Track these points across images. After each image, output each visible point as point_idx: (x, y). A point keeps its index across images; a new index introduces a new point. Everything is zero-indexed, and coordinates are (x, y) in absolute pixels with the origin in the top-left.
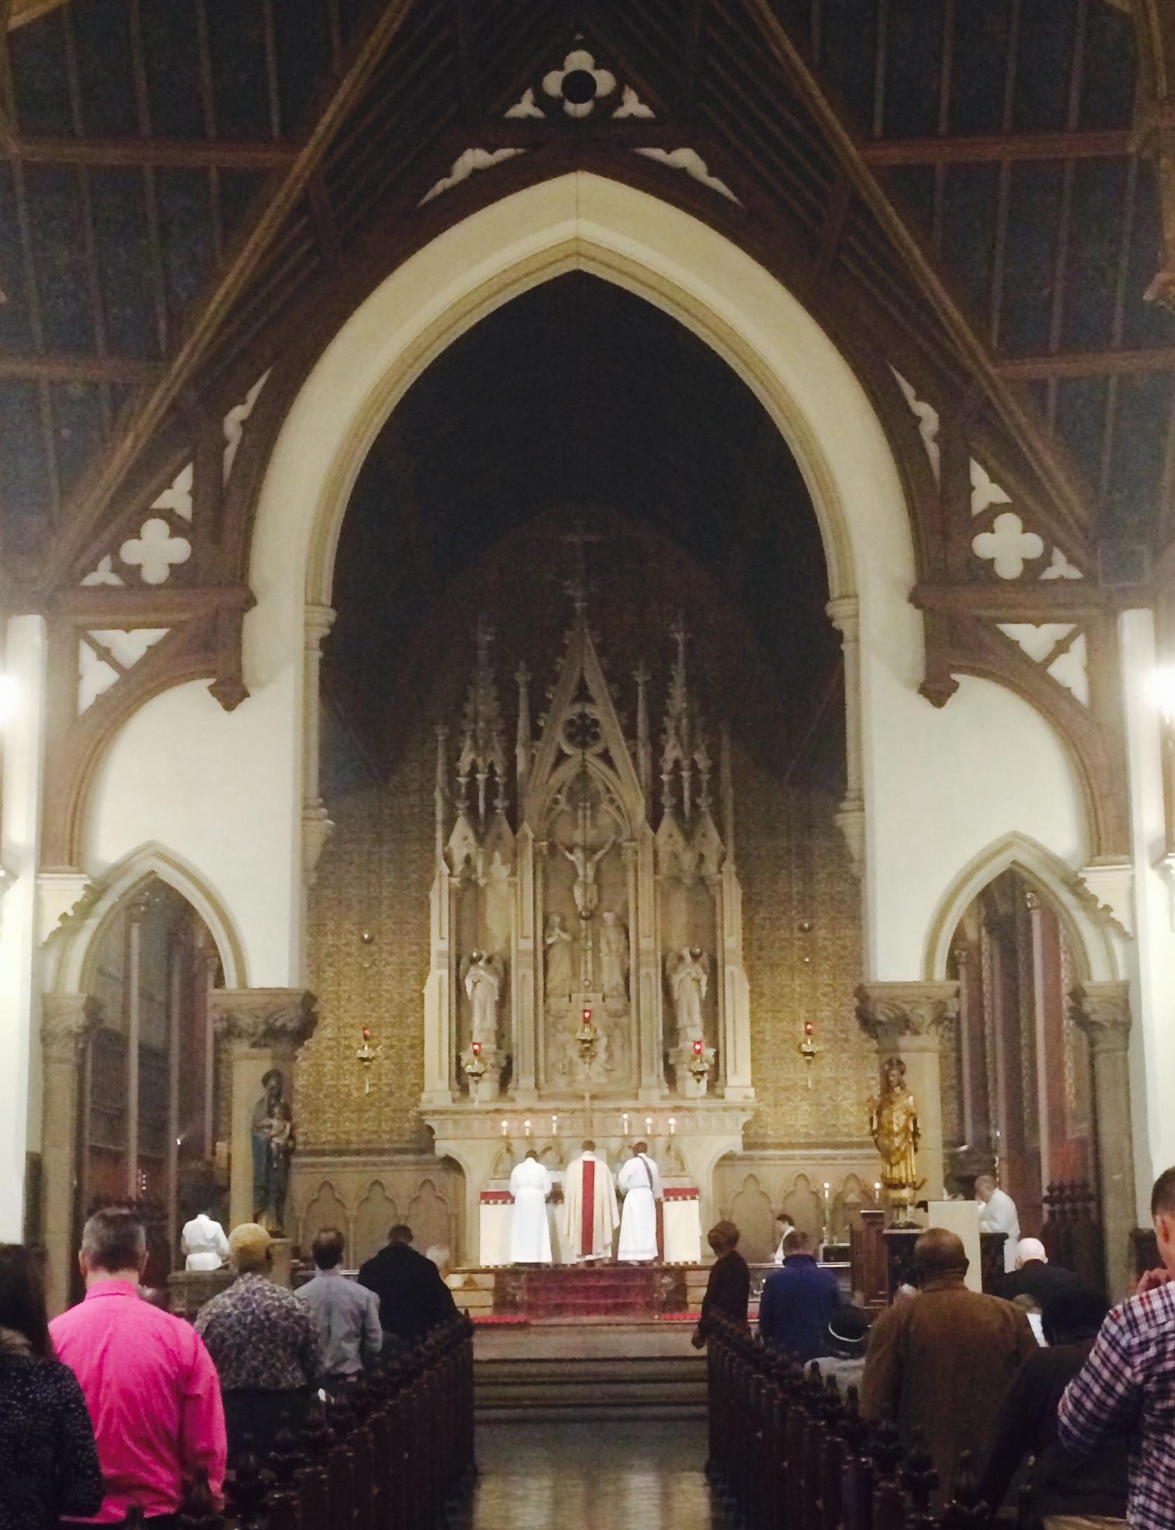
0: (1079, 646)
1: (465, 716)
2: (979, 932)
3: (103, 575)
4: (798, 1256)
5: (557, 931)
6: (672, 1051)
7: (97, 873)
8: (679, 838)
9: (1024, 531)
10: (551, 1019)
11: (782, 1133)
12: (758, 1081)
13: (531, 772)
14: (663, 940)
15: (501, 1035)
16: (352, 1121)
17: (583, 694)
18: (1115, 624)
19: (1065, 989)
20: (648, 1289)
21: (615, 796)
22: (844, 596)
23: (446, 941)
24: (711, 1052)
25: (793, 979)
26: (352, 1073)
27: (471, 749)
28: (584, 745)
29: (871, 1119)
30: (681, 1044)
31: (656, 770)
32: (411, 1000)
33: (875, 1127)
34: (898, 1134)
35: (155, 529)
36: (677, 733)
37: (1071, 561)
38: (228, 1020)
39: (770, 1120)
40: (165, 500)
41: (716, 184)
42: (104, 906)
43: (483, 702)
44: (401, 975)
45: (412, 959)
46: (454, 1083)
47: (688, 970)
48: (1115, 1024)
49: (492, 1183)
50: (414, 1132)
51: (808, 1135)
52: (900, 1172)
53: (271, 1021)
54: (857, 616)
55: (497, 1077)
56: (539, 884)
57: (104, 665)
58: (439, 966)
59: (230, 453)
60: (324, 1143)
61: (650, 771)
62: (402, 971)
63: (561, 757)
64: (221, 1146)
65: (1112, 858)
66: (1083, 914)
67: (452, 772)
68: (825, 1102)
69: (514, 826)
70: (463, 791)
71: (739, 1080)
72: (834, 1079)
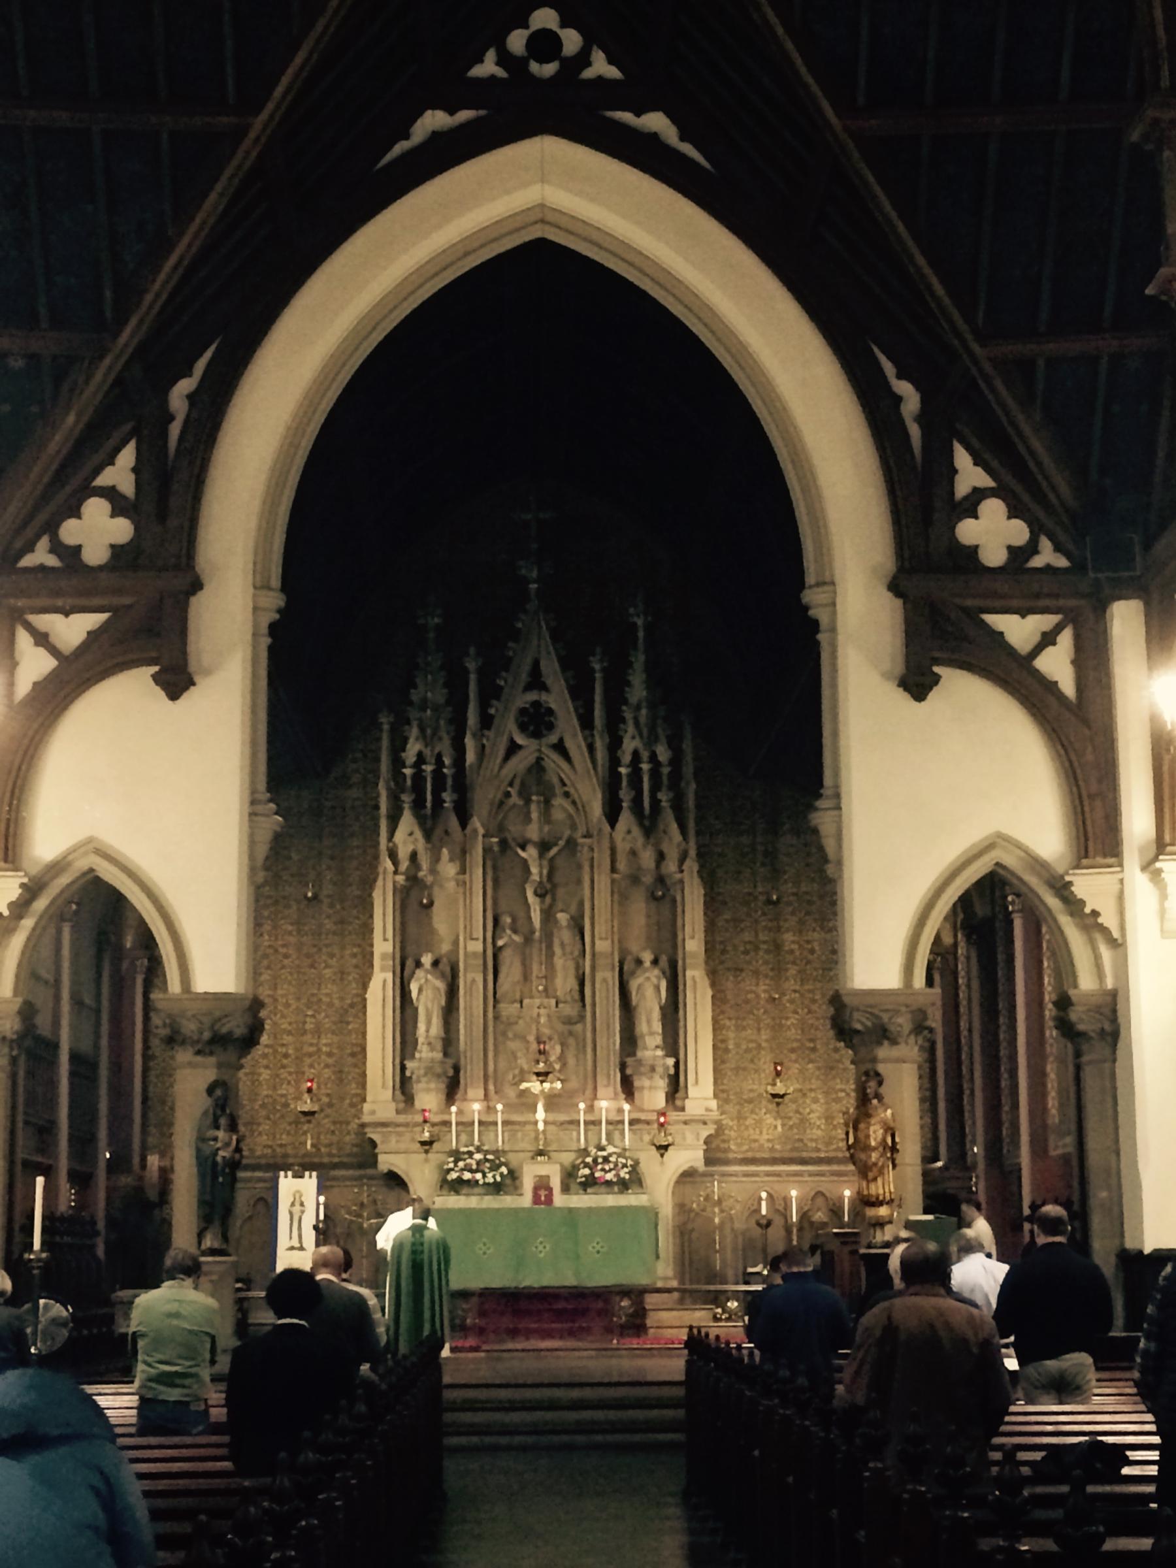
0: (1066, 638)
1: (411, 703)
2: (955, 936)
3: (41, 556)
4: (799, 1273)
5: (508, 932)
6: (629, 1060)
7: (34, 870)
8: (637, 832)
9: (1009, 518)
10: (501, 1027)
11: (745, 1147)
12: (719, 1093)
13: (480, 766)
14: (620, 941)
15: (449, 1042)
16: (288, 1133)
17: (536, 682)
18: (1105, 611)
19: (1049, 997)
20: (606, 1313)
21: (572, 791)
22: (818, 584)
23: (391, 942)
24: (671, 1061)
25: (757, 984)
26: (289, 1083)
27: (417, 739)
28: (537, 735)
29: (847, 1134)
30: (639, 1054)
31: (614, 762)
32: (352, 1006)
33: (851, 1141)
34: (875, 1149)
35: (96, 509)
36: (637, 724)
37: (1058, 548)
38: (171, 1025)
39: (733, 1134)
40: (106, 478)
41: (688, 149)
42: (41, 904)
43: (430, 690)
44: (342, 979)
45: (354, 961)
46: (398, 1093)
47: (647, 974)
48: (1102, 1033)
49: (437, 1199)
50: (356, 1145)
51: (772, 1149)
52: (876, 1189)
53: (216, 1028)
54: (834, 604)
55: (443, 1086)
56: (490, 883)
57: (41, 652)
58: (383, 969)
59: (175, 429)
60: (259, 1157)
61: (607, 765)
62: (342, 973)
63: (513, 749)
64: (153, 1161)
65: (1100, 860)
66: (1069, 918)
67: (397, 763)
68: (791, 1114)
69: (464, 821)
70: (409, 782)
71: (701, 1093)
72: (801, 1090)
